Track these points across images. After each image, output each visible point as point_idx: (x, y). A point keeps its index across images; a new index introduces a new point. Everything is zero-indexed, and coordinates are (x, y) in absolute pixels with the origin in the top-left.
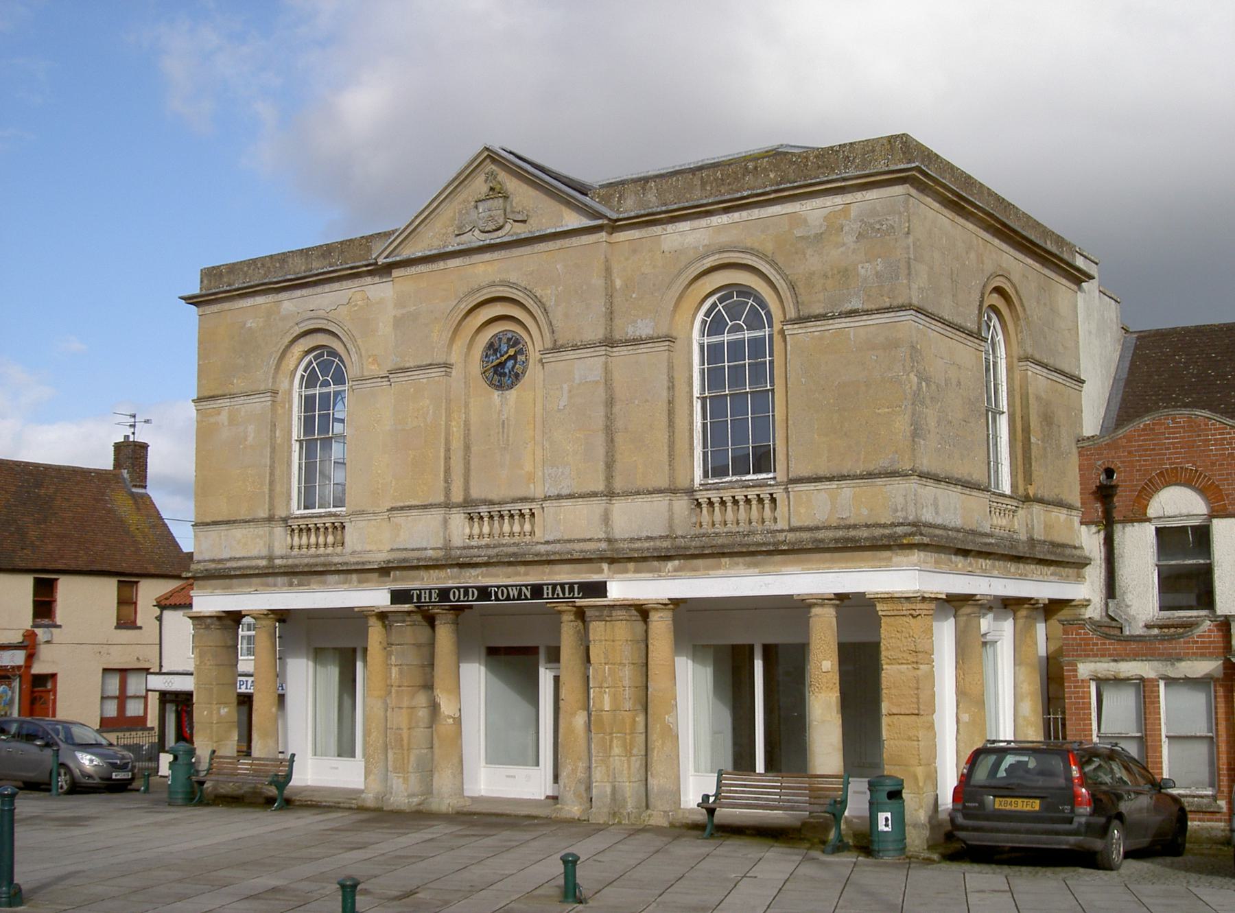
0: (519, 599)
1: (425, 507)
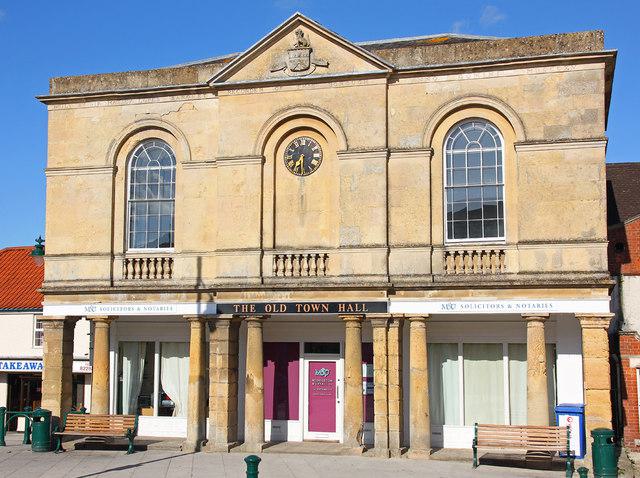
0: (320, 311)
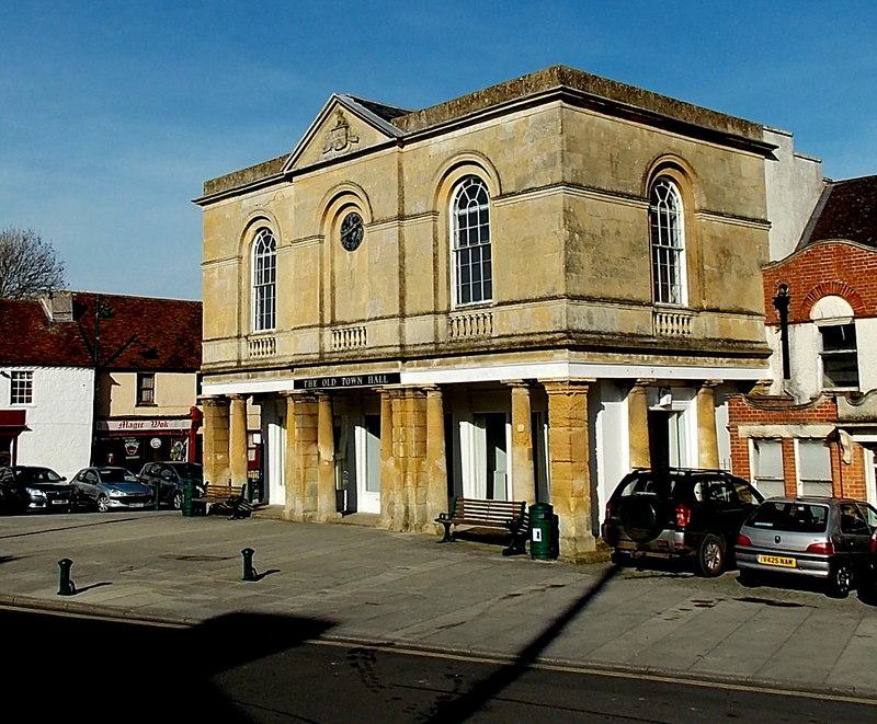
1: (310, 327)
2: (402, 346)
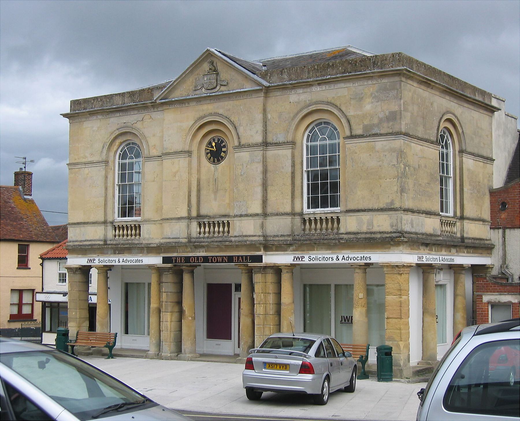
0: (222, 262)
2: (264, 236)
